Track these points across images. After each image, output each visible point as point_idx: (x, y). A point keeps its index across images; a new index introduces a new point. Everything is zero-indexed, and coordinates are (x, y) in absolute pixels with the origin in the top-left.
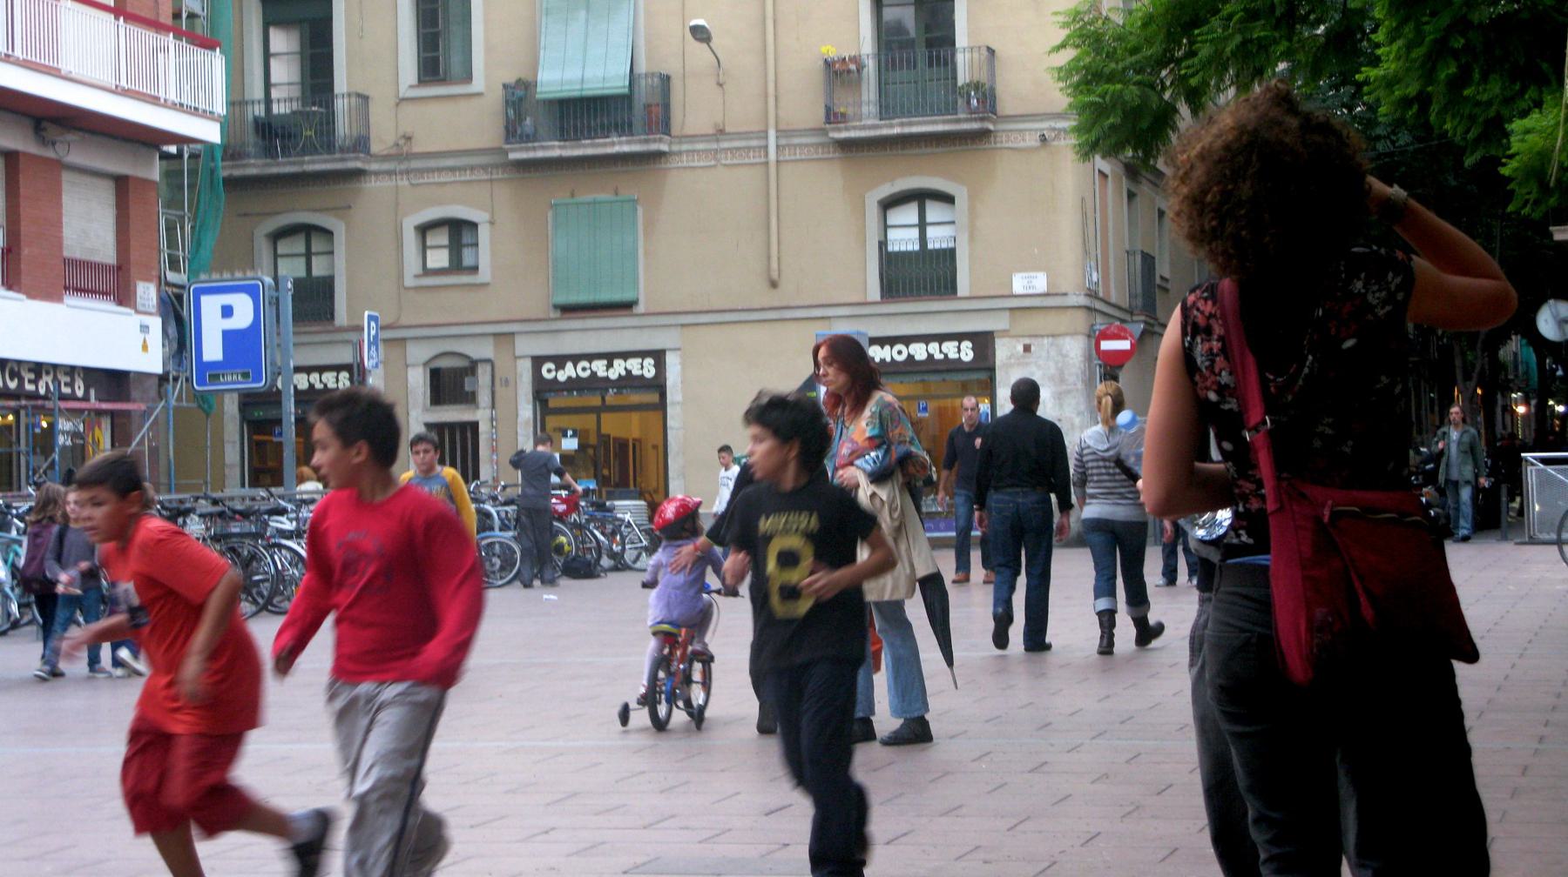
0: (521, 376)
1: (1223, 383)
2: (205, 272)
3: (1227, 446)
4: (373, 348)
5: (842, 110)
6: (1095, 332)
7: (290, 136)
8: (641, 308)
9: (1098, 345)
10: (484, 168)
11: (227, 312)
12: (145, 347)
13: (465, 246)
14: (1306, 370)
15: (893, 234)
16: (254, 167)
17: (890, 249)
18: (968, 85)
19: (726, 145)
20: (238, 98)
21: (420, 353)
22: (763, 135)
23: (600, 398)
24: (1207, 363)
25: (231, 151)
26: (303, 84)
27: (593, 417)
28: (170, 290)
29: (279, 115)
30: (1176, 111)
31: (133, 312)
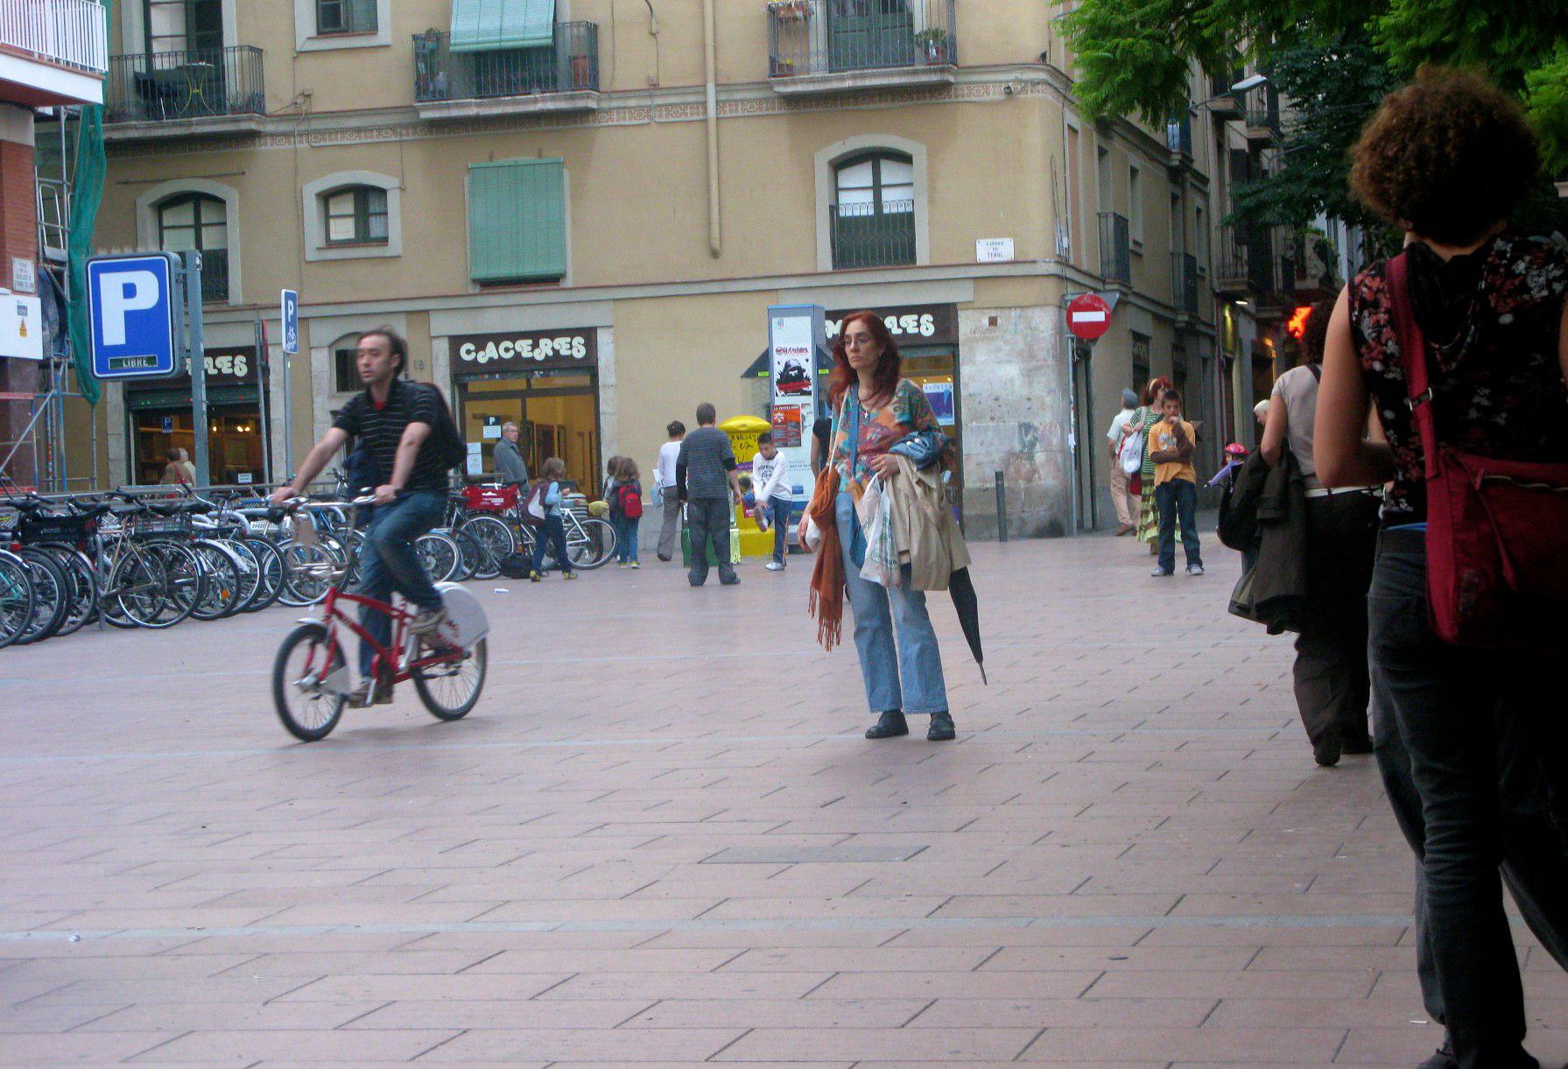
0: (437, 358)
1: (1388, 352)
2: (103, 246)
3: (1389, 414)
4: (292, 330)
5: (788, 61)
6: (1066, 302)
7: (175, 94)
8: (569, 282)
9: (1069, 317)
10: (392, 128)
11: (129, 291)
12: (23, 331)
13: (371, 215)
14: (1469, 339)
15: (845, 198)
16: (136, 129)
17: (842, 214)
18: (926, 33)
19: (659, 101)
20: (117, 53)
21: (324, 334)
22: (701, 89)
23: (524, 381)
24: (1374, 335)
25: (112, 112)
26: (187, 35)
27: (518, 402)
28: (49, 267)
29: (162, 71)
30: (1186, 66)
31: (9, 291)
